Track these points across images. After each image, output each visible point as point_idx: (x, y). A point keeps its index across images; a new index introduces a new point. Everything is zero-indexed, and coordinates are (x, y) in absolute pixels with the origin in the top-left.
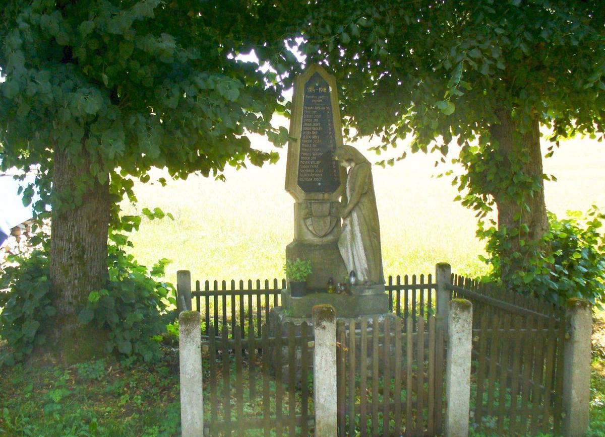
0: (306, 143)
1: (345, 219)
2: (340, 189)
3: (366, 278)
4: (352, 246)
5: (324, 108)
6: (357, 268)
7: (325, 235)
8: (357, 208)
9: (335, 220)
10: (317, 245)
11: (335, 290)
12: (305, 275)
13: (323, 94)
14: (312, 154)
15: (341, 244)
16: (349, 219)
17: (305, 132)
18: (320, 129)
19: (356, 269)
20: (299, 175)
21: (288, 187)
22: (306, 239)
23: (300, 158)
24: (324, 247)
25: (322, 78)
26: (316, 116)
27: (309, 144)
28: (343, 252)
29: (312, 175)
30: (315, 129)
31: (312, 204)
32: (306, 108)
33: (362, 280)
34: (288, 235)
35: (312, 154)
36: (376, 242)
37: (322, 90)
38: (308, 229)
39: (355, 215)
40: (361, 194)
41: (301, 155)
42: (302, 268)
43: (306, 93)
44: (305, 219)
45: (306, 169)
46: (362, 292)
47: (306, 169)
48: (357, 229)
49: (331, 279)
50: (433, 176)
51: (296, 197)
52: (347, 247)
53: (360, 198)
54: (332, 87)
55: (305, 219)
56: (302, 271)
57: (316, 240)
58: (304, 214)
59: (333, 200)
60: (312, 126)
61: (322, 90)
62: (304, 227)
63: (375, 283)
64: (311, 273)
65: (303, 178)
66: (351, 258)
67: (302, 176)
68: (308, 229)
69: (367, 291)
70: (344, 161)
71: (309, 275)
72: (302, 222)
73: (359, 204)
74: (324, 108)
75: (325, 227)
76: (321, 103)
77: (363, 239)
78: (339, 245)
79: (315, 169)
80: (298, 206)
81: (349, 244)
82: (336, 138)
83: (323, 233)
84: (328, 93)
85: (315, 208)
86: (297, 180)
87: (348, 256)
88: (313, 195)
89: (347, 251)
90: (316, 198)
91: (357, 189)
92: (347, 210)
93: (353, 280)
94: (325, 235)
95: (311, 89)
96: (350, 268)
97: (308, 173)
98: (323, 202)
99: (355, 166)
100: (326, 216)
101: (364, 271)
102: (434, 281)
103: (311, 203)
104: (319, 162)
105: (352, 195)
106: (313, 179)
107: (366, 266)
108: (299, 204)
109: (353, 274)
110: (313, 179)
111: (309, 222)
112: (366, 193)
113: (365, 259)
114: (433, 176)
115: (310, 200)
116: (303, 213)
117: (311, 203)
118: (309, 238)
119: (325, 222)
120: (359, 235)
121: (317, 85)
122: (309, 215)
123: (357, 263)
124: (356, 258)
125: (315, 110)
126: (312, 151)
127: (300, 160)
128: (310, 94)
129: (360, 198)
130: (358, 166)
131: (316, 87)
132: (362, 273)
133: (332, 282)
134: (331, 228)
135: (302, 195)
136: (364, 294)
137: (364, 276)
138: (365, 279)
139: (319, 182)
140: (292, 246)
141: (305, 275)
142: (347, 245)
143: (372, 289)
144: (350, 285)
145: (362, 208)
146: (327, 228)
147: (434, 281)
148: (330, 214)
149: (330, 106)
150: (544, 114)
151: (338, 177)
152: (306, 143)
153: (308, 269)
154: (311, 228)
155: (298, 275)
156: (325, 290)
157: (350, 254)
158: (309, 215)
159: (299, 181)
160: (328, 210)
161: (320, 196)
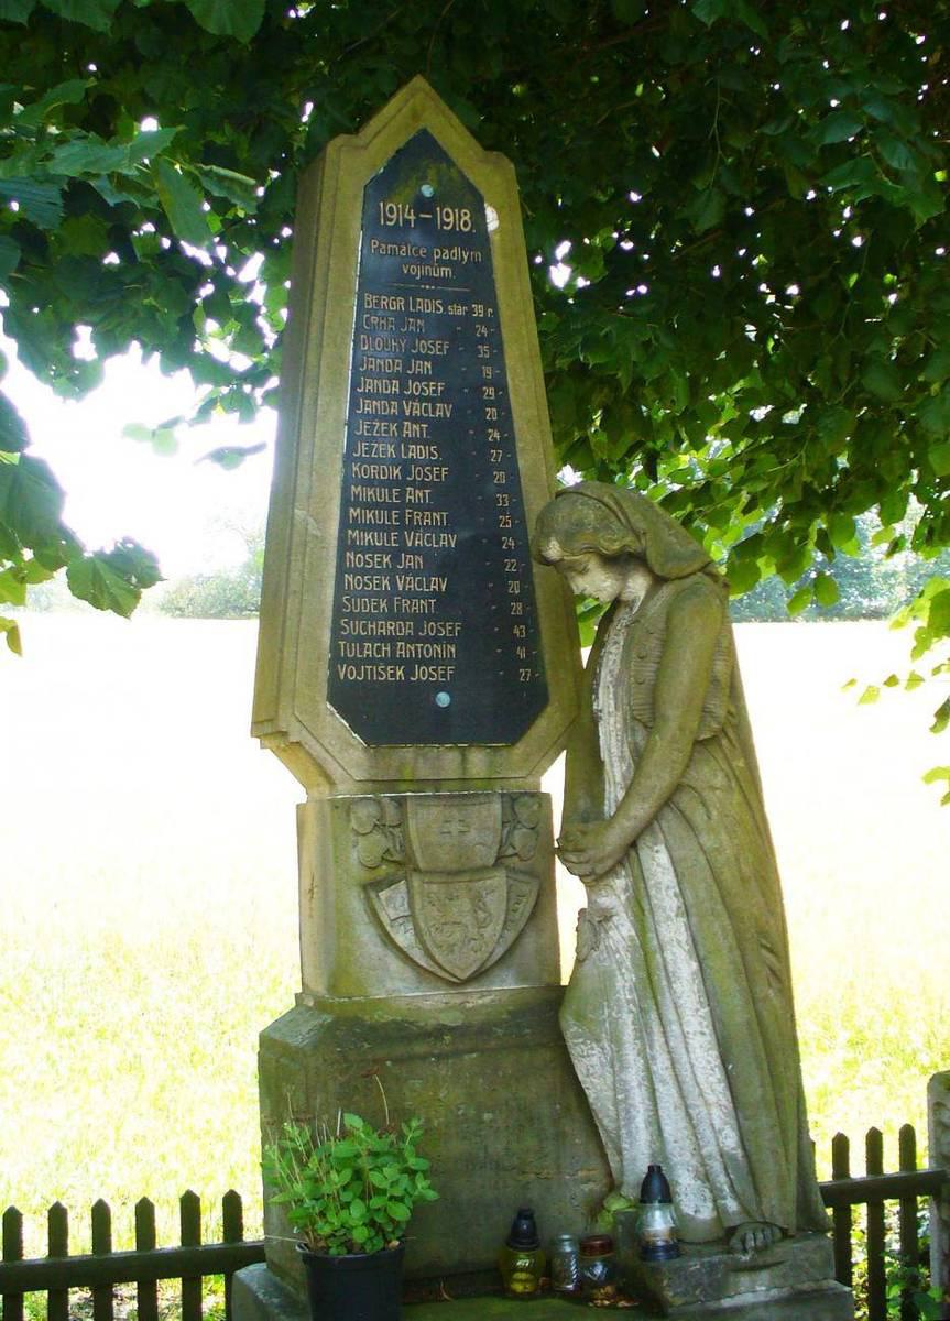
0: (369, 483)
1: (593, 879)
2: (547, 724)
3: (732, 1205)
4: (643, 1032)
5: (460, 311)
6: (671, 1147)
7: (480, 975)
8: (670, 821)
9: (529, 889)
10: (440, 1031)
11: (548, 1276)
12: (401, 1212)
13: (455, 238)
14: (401, 540)
15: (580, 1018)
16: (620, 883)
17: (363, 428)
18: (443, 410)
19: (666, 1159)
20: (335, 648)
21: (268, 725)
22: (379, 994)
23: (341, 557)
24: (472, 1035)
25: (450, 163)
26: (422, 346)
27: (390, 484)
28: (590, 1064)
29: (405, 650)
30: (418, 409)
31: (410, 806)
32: (370, 299)
33: (706, 1213)
34: (270, 977)
35: (401, 540)
36: (776, 1001)
37: (454, 218)
38: (388, 940)
39: (658, 862)
40: (698, 743)
41: (344, 546)
42: (385, 1177)
43: (372, 226)
44: (372, 886)
45: (372, 618)
46: (719, 1290)
47: (372, 618)
48: (673, 933)
49: (525, 1214)
50: (852, 682)
51: (313, 769)
52: (616, 1040)
53: (689, 763)
54: (499, 211)
55: (372, 886)
56: (380, 1192)
57: (433, 1003)
58: (365, 862)
59: (513, 787)
60: (400, 397)
61: (454, 218)
62: (366, 934)
63: (785, 1234)
64: (432, 1195)
65: (357, 663)
66: (639, 1097)
67: (353, 652)
68: (388, 940)
69: (744, 1280)
70: (593, 564)
71: (419, 1209)
72: (356, 905)
73: (685, 800)
74: (460, 311)
75: (481, 925)
76: (443, 281)
77: (710, 996)
78: (571, 1029)
79: (419, 619)
80: (325, 825)
81: (628, 1018)
82: (521, 463)
83: (464, 966)
84: (477, 238)
85: (426, 824)
86: (324, 673)
87: (619, 1086)
88: (413, 760)
89: (616, 1063)
90: (424, 772)
91: (674, 714)
92: (614, 838)
93: (659, 1223)
94: (480, 975)
95: (398, 210)
96: (638, 1157)
97: (382, 639)
98: (464, 793)
99: (650, 595)
100: (481, 870)
101: (716, 1166)
102: (923, 1163)
103: (401, 803)
104: (438, 584)
105: (639, 757)
106: (409, 672)
107: (730, 1140)
108: (335, 805)
109: (657, 1187)
110: (409, 672)
111: (393, 903)
112: (714, 739)
113: (725, 1100)
114: (852, 682)
115: (391, 784)
116: (360, 852)
117: (401, 803)
118: (396, 990)
119: (478, 901)
120: (683, 966)
121: (427, 191)
122: (397, 866)
123: (673, 1125)
124: (667, 1094)
125: (418, 315)
126: (403, 527)
127: (342, 569)
128: (398, 233)
129: (689, 763)
130: (666, 591)
131: (421, 204)
132: (706, 1177)
133: (525, 1231)
134: (511, 935)
135: (349, 755)
136: (726, 1303)
137: (716, 1197)
138: (719, 1209)
139: (440, 687)
140: (300, 1038)
141: (401, 1212)
142: (615, 1022)
143: (766, 1267)
144: (647, 1250)
145: (699, 817)
146: (493, 936)
147: (923, 1163)
148: (500, 860)
149: (491, 300)
150: (906, 527)
151: (534, 661)
152: (369, 483)
153: (412, 1173)
154: (404, 938)
155: (357, 1212)
156: (494, 1280)
157: (634, 1075)
158: (397, 866)
159: (333, 679)
160: (491, 839)
161: (447, 761)
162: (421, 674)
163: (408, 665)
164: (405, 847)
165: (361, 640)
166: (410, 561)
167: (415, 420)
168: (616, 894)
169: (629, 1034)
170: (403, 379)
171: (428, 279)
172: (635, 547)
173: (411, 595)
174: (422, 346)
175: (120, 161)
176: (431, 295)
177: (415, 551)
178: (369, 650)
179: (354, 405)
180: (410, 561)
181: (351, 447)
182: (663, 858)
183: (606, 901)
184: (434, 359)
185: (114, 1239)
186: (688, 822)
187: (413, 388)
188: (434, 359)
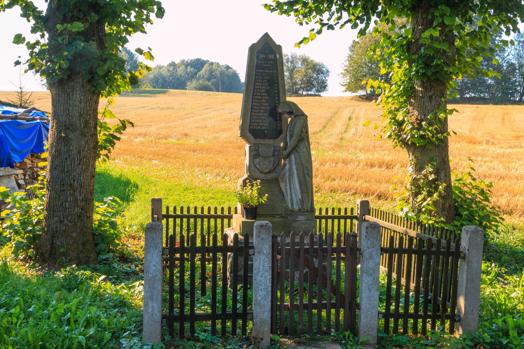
3: (300, 206)
7: (269, 172)
17: (255, 90)
26: (265, 77)
28: (282, 185)
30: (264, 87)
39: (293, 157)
40: (299, 140)
48: (294, 167)
63: (307, 211)
66: (289, 190)
77: (298, 176)
87: (286, 189)
107: (300, 197)
120: (295, 175)
126: (261, 106)
127: (251, 112)
138: (299, 207)
142: (286, 180)
154: (258, 166)
159: (249, 128)
162: (263, 128)
163: (261, 126)
164: (259, 153)
165: (254, 123)
166: (262, 111)
167: (263, 109)
168: (287, 162)
169: (288, 181)
170: (262, 83)
171: (266, 67)
172: (291, 111)
173: (262, 116)
174: (265, 77)
175: (80, 155)
176: (267, 69)
177: (263, 109)
178: (255, 124)
179: (254, 87)
180: (262, 111)
181: (254, 93)
182: (293, 156)
183: (286, 162)
184: (267, 80)
185: (241, 100)
186: (297, 152)
187: (264, 84)
188: (267, 80)
